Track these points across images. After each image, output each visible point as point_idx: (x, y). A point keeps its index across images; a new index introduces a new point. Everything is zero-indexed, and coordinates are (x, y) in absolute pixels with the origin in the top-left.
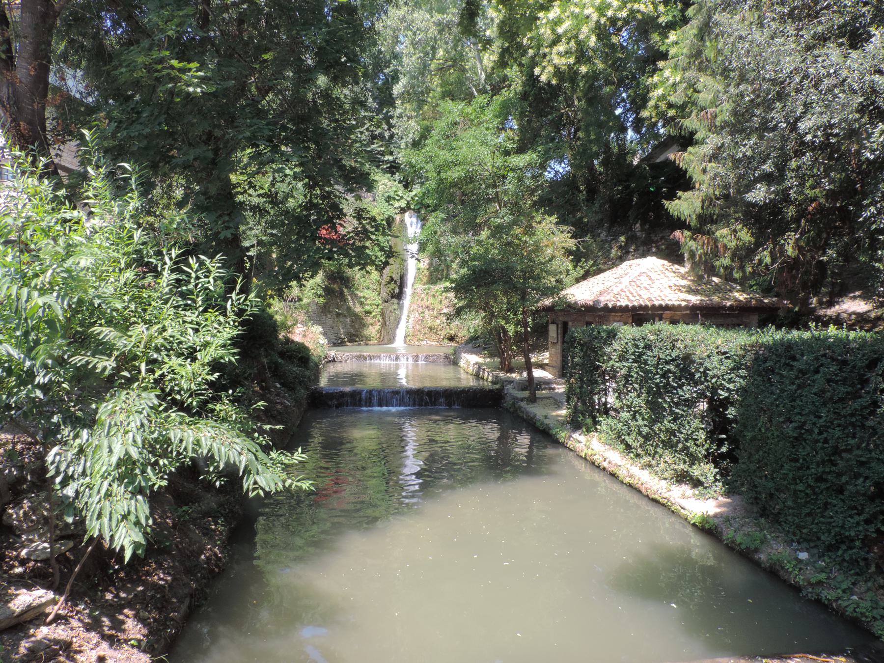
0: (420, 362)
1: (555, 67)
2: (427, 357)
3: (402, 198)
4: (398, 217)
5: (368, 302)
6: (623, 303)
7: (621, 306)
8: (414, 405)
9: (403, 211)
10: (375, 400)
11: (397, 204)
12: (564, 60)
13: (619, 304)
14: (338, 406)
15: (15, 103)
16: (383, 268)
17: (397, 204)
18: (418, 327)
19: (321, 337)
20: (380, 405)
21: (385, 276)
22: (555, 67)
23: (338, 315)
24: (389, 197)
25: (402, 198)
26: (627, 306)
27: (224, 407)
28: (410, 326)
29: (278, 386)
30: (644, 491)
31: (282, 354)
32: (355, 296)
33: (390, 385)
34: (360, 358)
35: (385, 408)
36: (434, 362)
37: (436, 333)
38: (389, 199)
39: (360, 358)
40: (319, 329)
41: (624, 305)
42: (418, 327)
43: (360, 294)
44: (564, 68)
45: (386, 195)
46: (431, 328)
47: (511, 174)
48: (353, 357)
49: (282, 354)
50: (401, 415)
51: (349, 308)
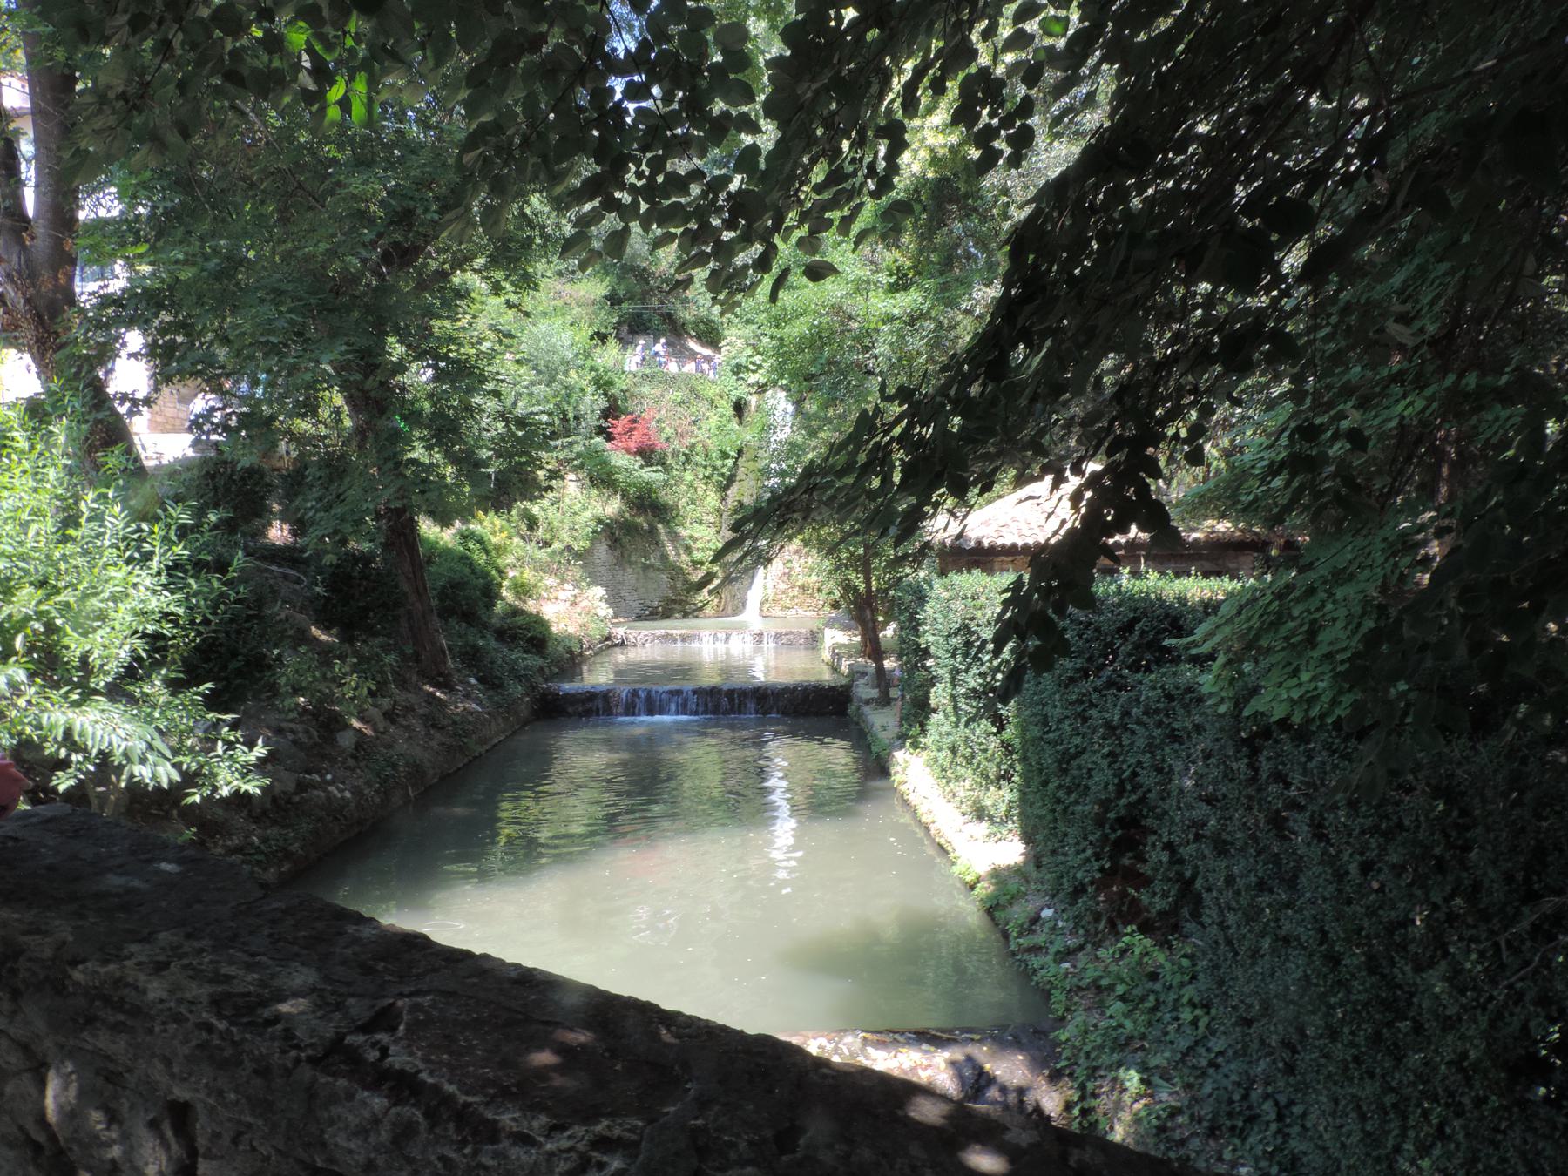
0: (765, 645)
1: (932, 150)
2: (778, 636)
3: (760, 367)
4: (753, 400)
5: (699, 545)
6: (1008, 541)
7: (1003, 546)
8: (705, 712)
9: (761, 389)
10: (640, 704)
11: (752, 379)
12: (941, 139)
13: (1000, 542)
14: (588, 713)
15: (29, 276)
16: (727, 487)
17: (752, 379)
18: (782, 586)
19: (604, 605)
20: (651, 713)
21: (729, 501)
22: (932, 150)
23: (646, 568)
24: (738, 366)
25: (760, 367)
26: (1014, 546)
27: (155, 687)
28: (770, 586)
29: (473, 681)
30: (933, 832)
31: (501, 634)
32: (675, 537)
33: (738, 681)
34: (667, 638)
35: (657, 718)
36: (789, 644)
37: (812, 596)
38: (738, 370)
39: (667, 638)
40: (599, 591)
41: (1008, 542)
42: (782, 586)
43: (684, 533)
44: (941, 151)
45: (734, 362)
46: (803, 587)
47: (886, 328)
48: (656, 637)
49: (501, 634)
50: (683, 728)
51: (664, 557)
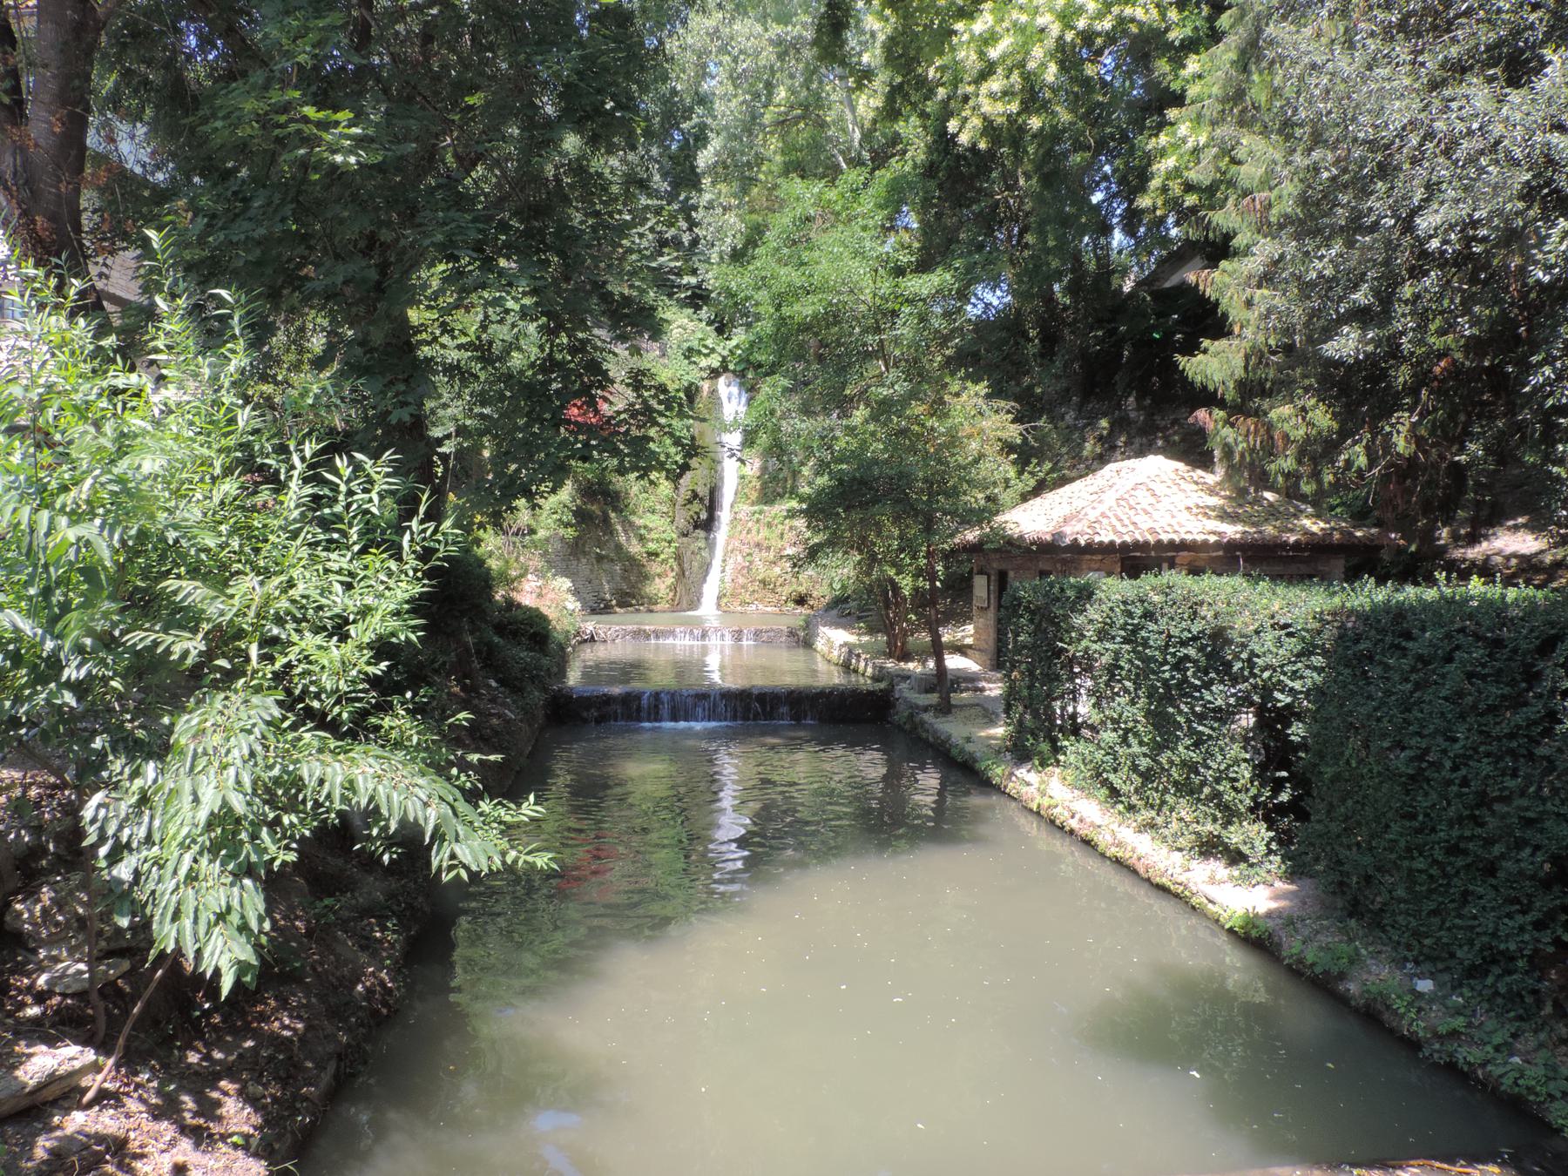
0: (745, 643)
1: (985, 118)
2: (757, 634)
3: (713, 350)
4: (706, 386)
5: (654, 535)
6: (1105, 537)
7: (1101, 543)
8: (734, 718)
9: (715, 373)
10: (665, 710)
11: (704, 363)
12: (1000, 107)
13: (1097, 539)
14: (600, 720)
15: (27, 183)
16: (680, 476)
17: (704, 363)
18: (741, 580)
19: (570, 597)
20: (675, 719)
21: (682, 490)
22: (985, 118)
23: (600, 558)
24: (690, 350)
25: (713, 350)
26: (1112, 543)
27: (397, 722)
28: (728, 579)
29: (494, 684)
30: (1141, 871)
31: (500, 629)
32: (629, 526)
33: (692, 684)
34: (639, 634)
35: (682, 724)
36: (769, 642)
37: (773, 591)
38: (689, 353)
39: (639, 634)
40: (565, 583)
41: (1106, 540)
42: (741, 580)
43: (639, 522)
44: (1000, 120)
45: (686, 345)
46: (764, 582)
47: (906, 309)
48: (626, 633)
49: (500, 629)
50: (711, 736)
51: (619, 547)
